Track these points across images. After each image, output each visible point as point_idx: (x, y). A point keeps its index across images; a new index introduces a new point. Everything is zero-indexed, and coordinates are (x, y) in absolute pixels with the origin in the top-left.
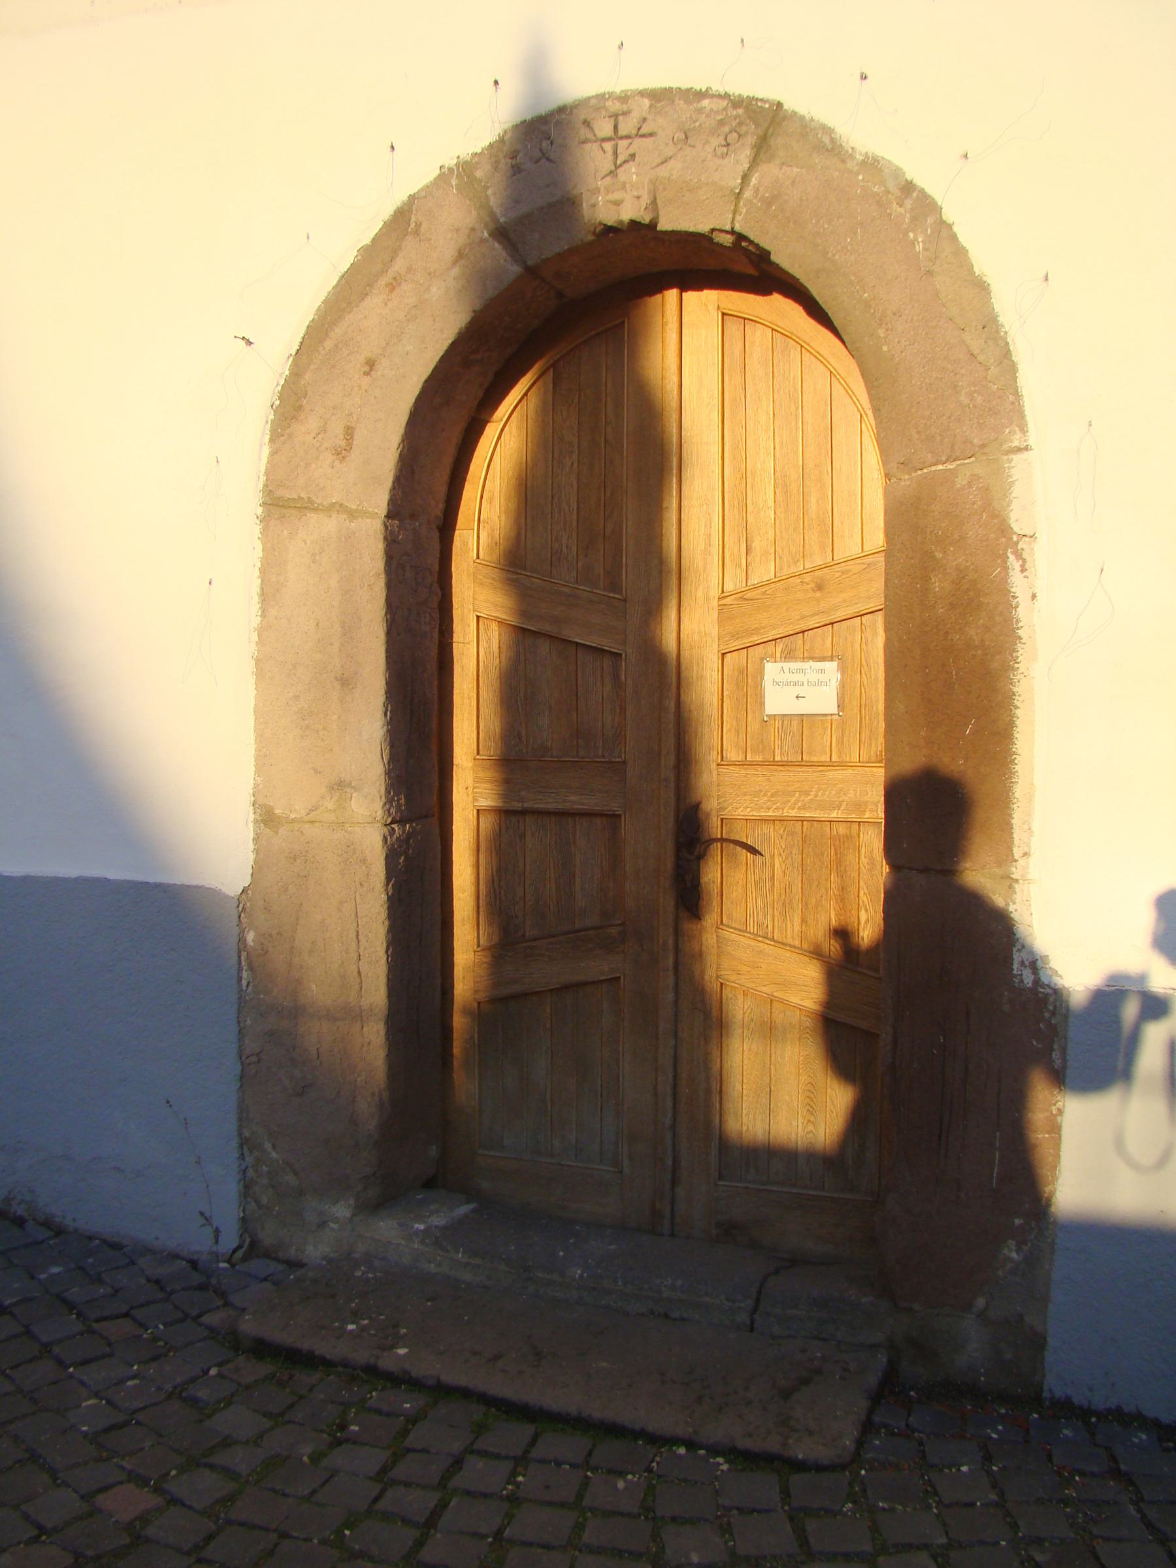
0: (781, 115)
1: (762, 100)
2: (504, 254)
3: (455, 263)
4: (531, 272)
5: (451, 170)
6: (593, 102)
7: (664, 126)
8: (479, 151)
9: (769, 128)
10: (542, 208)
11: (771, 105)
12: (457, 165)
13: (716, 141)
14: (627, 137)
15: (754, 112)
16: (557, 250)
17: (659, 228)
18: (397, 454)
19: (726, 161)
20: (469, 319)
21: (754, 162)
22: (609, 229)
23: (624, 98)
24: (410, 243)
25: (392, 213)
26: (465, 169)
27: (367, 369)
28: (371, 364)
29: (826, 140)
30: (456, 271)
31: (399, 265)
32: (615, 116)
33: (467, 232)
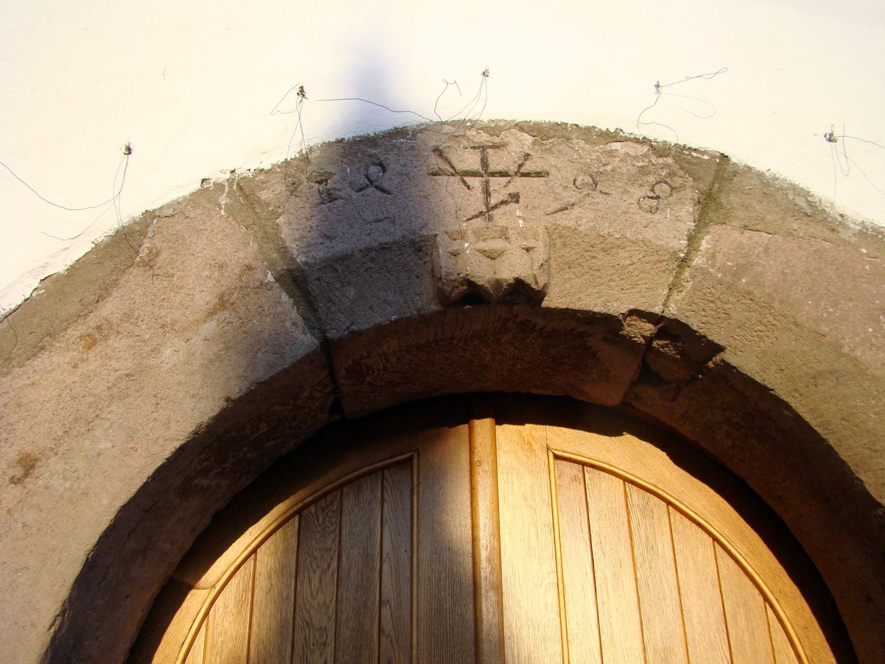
0: (730, 169)
1: (695, 150)
2: (294, 314)
3: (211, 314)
4: (328, 348)
5: (219, 187)
6: (447, 129)
7: (559, 164)
8: (267, 166)
9: (713, 183)
10: (369, 249)
11: (713, 157)
12: (230, 181)
13: (638, 192)
14: (502, 174)
15: (688, 162)
16: (379, 320)
17: (545, 304)
18: (47, 638)
19: (657, 217)
20: (217, 411)
21: (701, 223)
22: (474, 294)
23: (493, 129)
24: (135, 277)
25: (111, 233)
26: (243, 191)
27: (19, 472)
28: (28, 465)
29: (801, 202)
30: (210, 327)
31: (110, 308)
32: (483, 148)
33: (237, 271)
